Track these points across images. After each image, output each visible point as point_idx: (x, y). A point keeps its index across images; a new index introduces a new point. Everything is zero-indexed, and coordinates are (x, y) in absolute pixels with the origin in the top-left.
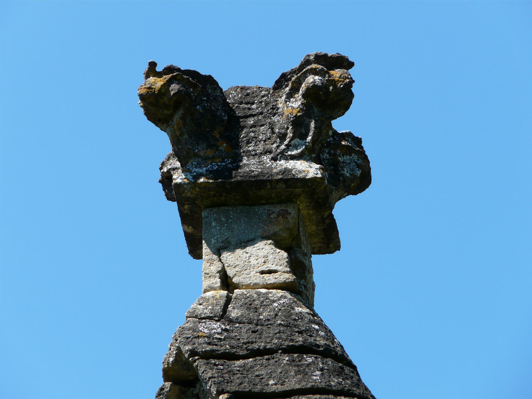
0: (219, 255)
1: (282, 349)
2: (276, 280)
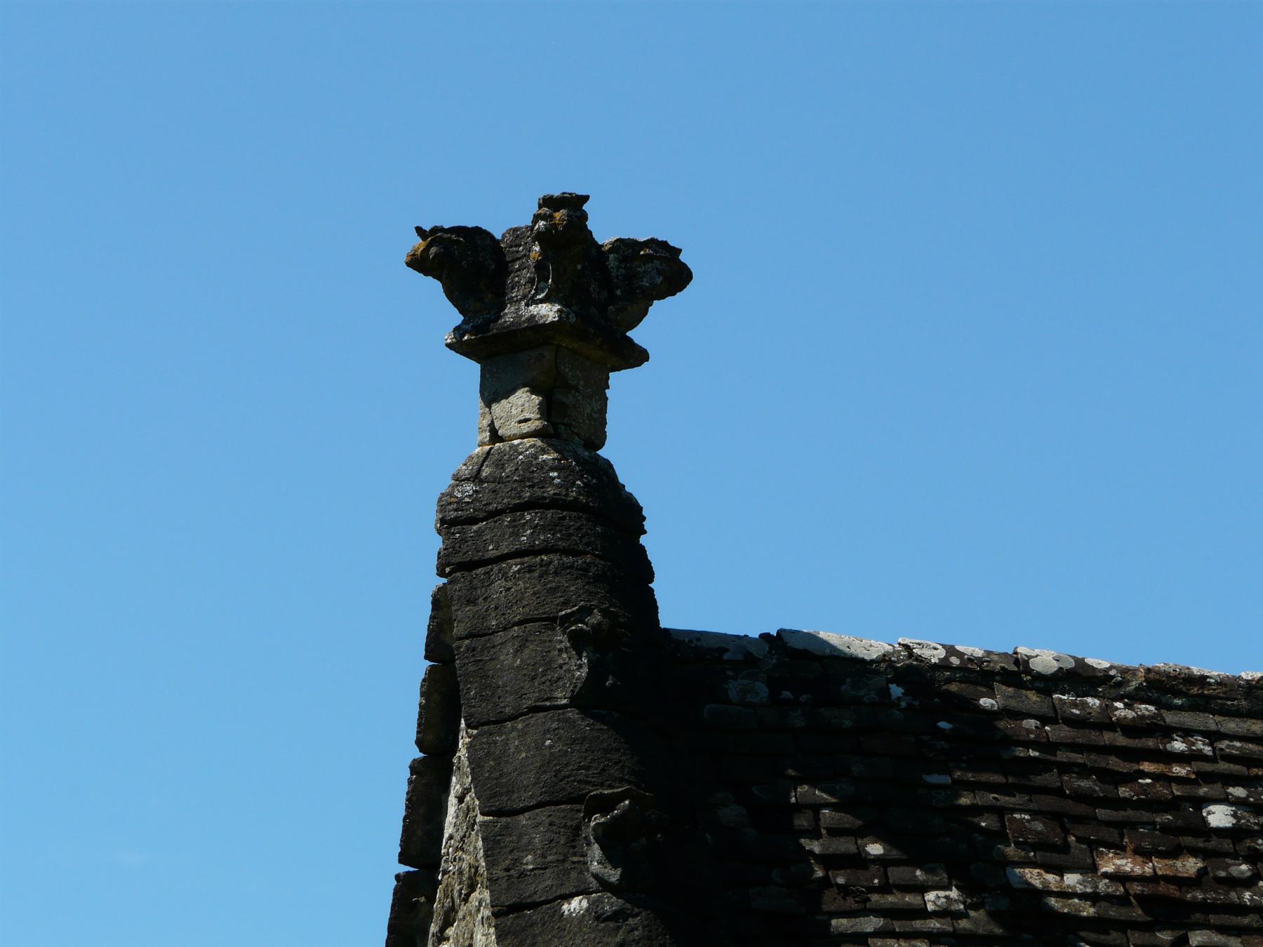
0: (490, 408)
2: (529, 429)
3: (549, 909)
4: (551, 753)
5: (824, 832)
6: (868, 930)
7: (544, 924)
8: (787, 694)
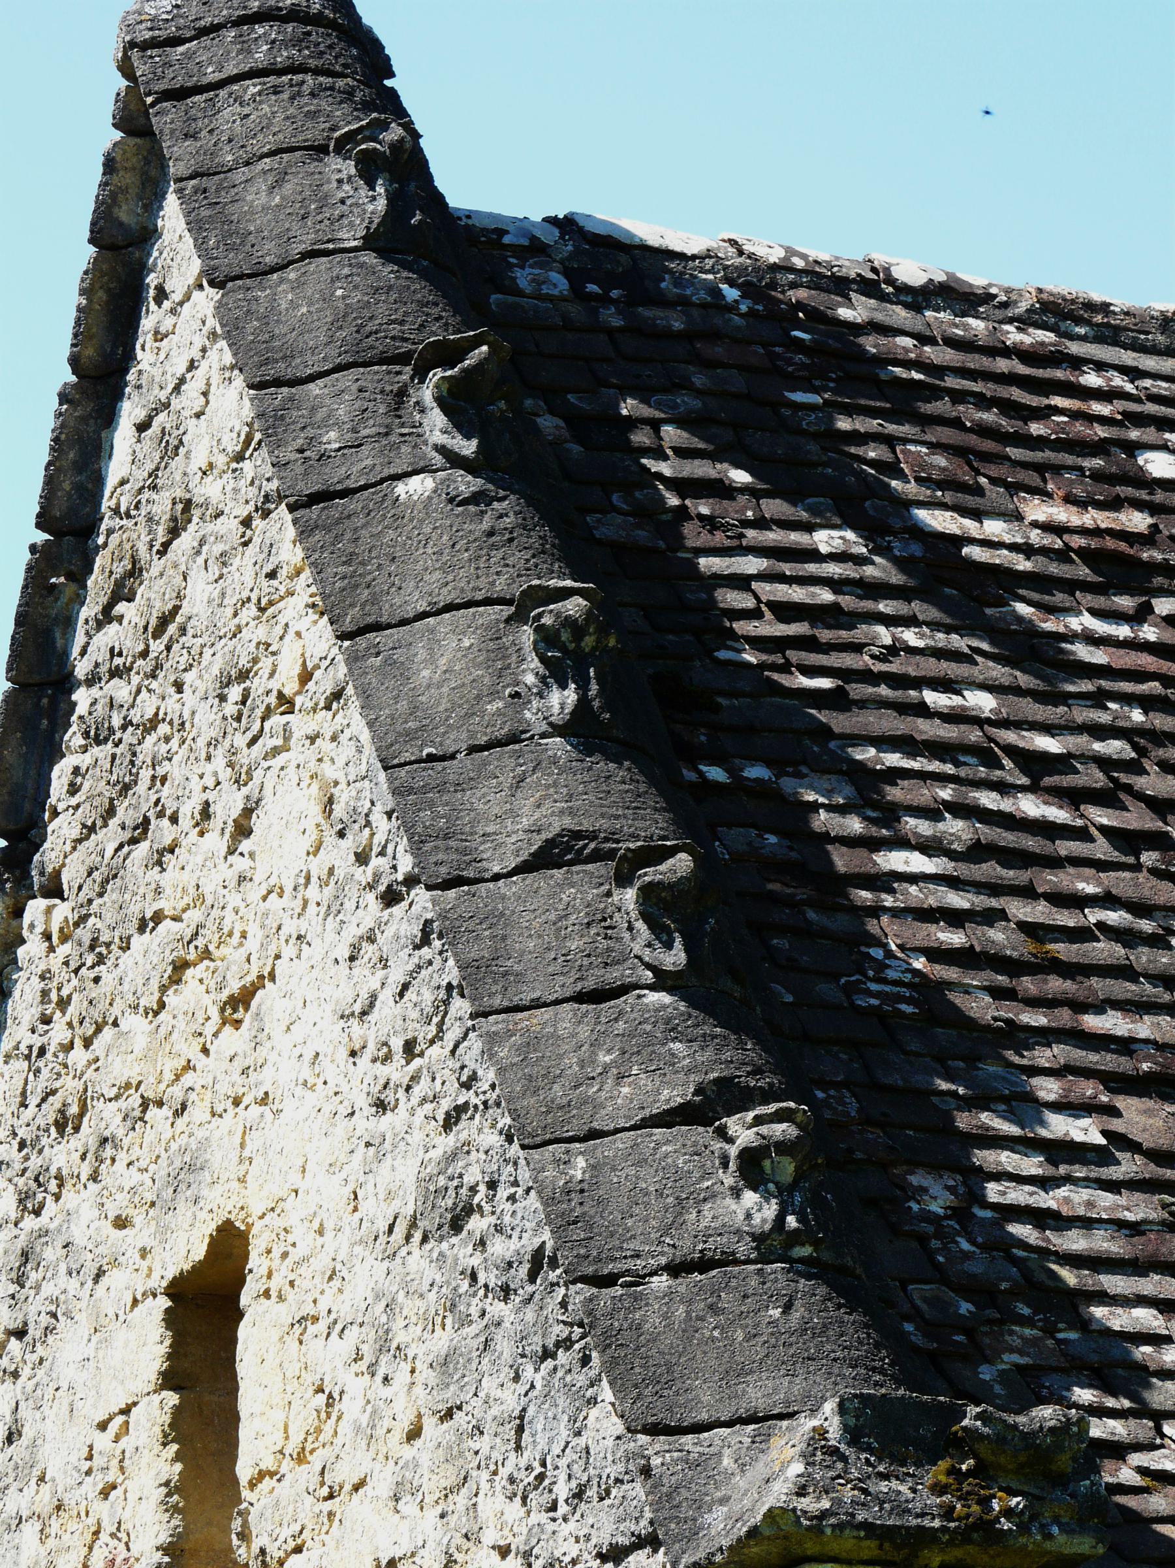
1: (231, 22)
3: (373, 494)
4: (347, 305)
5: (669, 452)
6: (750, 572)
7: (368, 514)
8: (592, 288)
